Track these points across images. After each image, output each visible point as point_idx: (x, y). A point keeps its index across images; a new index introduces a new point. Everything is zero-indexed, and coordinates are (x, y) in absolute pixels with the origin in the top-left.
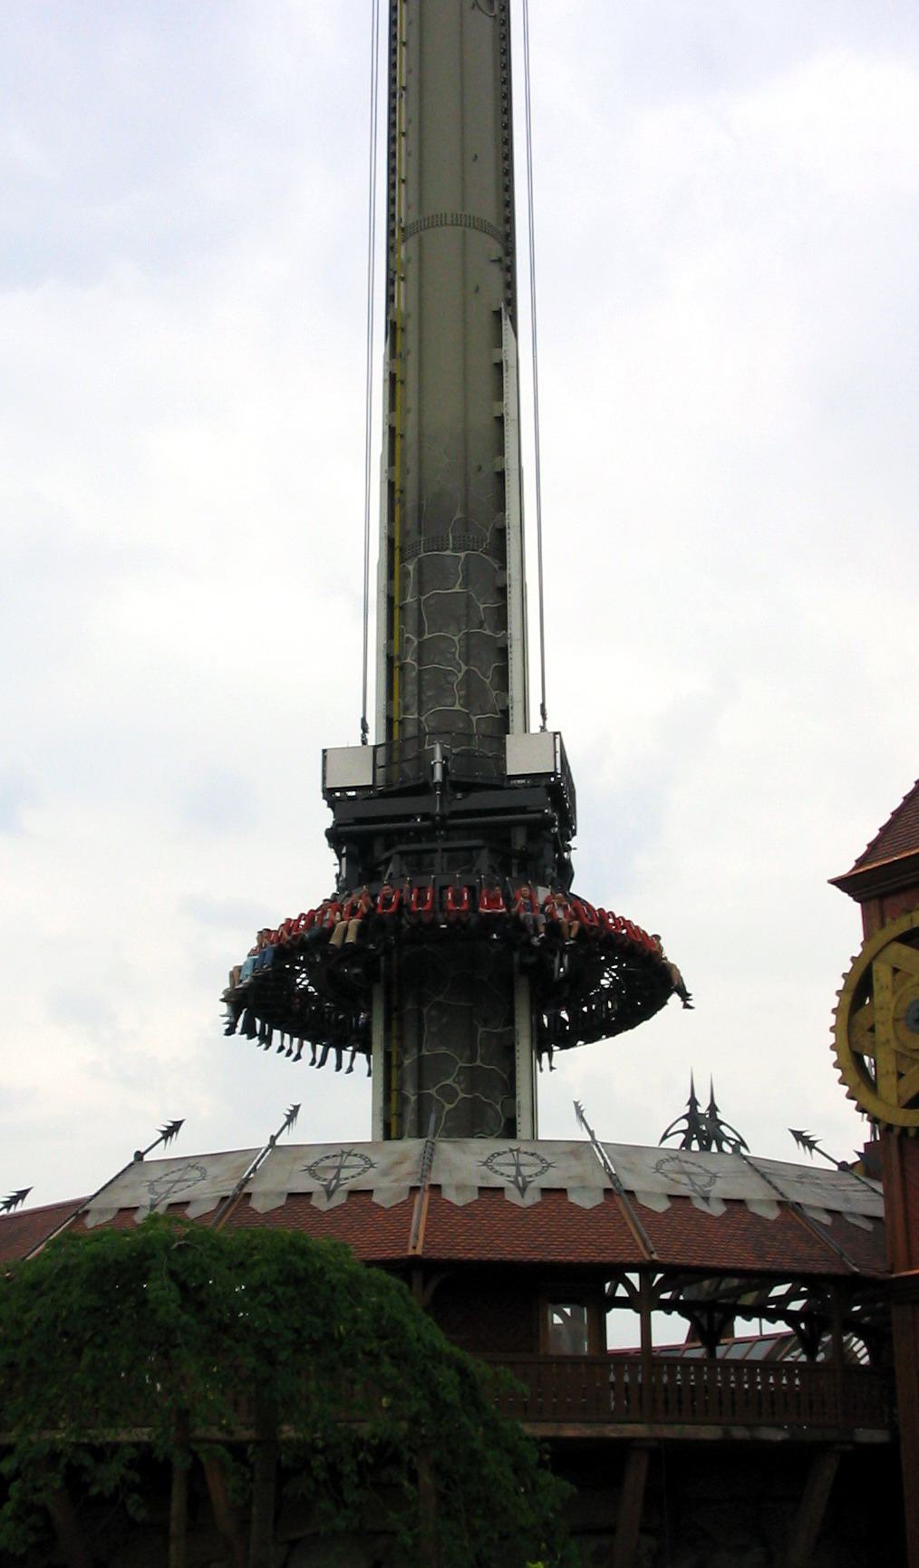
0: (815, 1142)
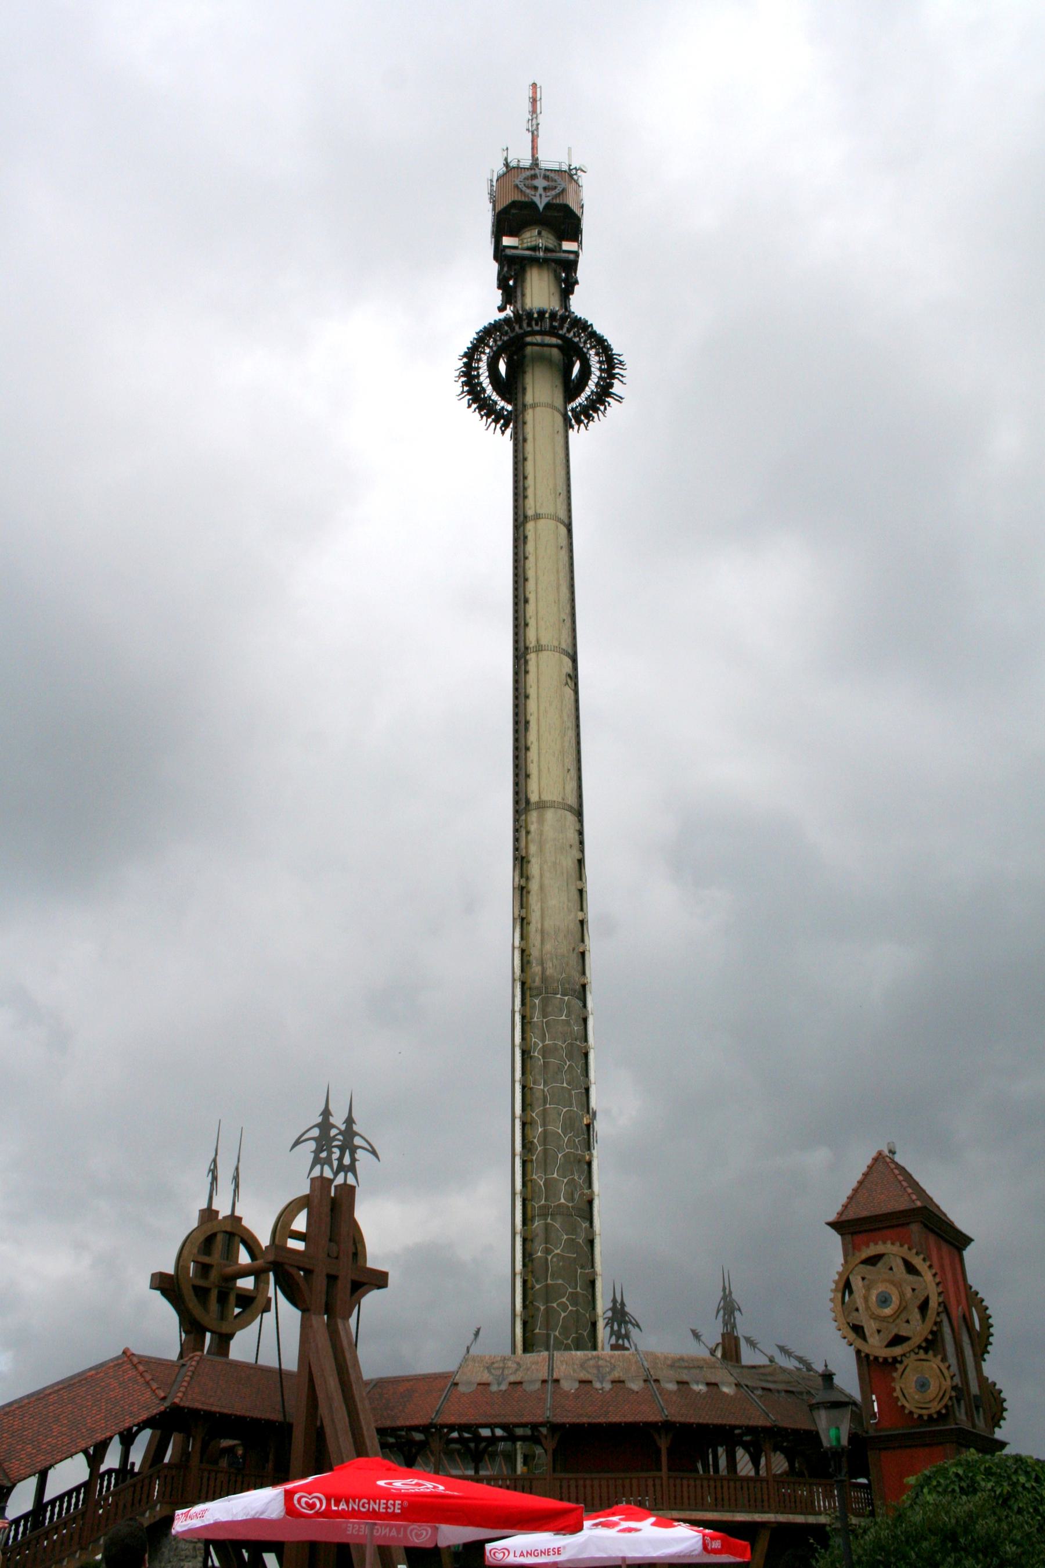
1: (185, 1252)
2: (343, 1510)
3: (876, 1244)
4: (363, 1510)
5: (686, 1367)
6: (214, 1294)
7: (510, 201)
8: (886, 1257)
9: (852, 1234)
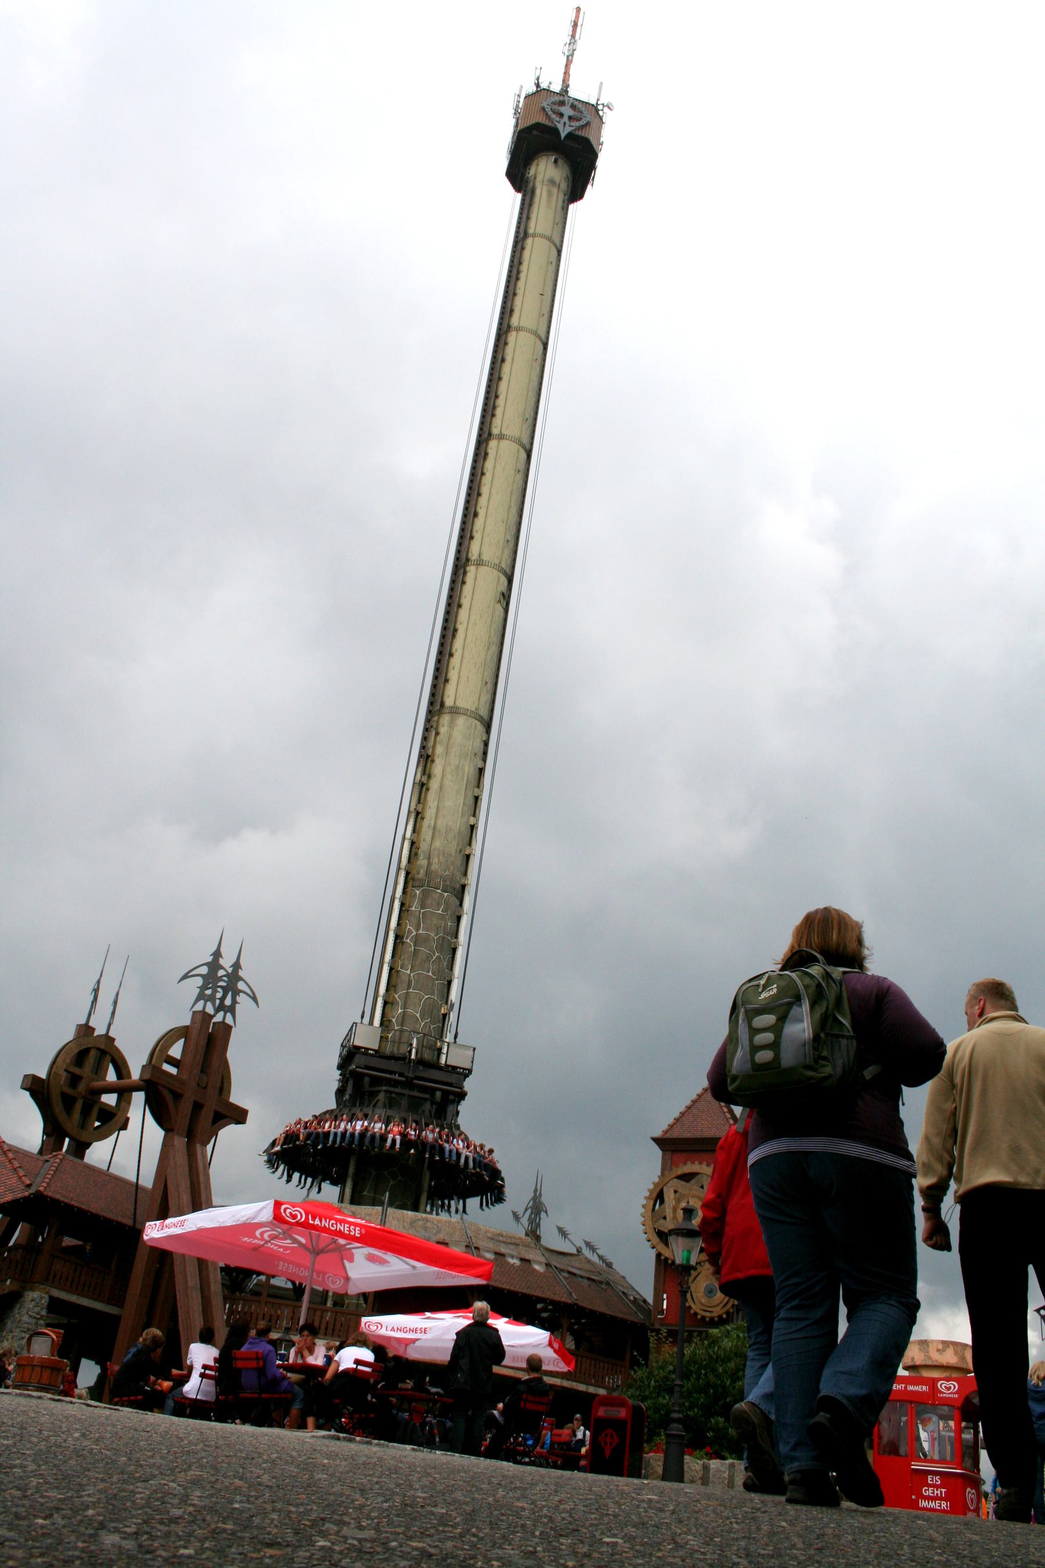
0: (596, 1249)
1: (59, 1059)
2: (318, 1225)
3: (693, 1163)
4: (333, 1229)
5: (504, 1242)
6: (79, 1106)
7: (534, 122)
8: (699, 1176)
9: (673, 1151)
